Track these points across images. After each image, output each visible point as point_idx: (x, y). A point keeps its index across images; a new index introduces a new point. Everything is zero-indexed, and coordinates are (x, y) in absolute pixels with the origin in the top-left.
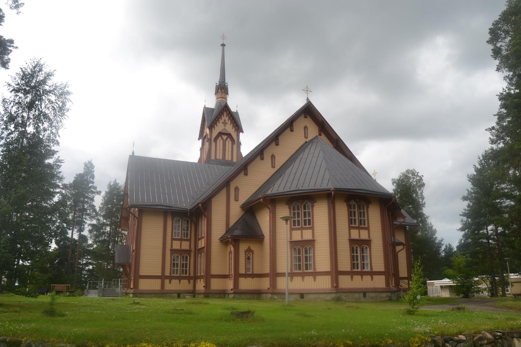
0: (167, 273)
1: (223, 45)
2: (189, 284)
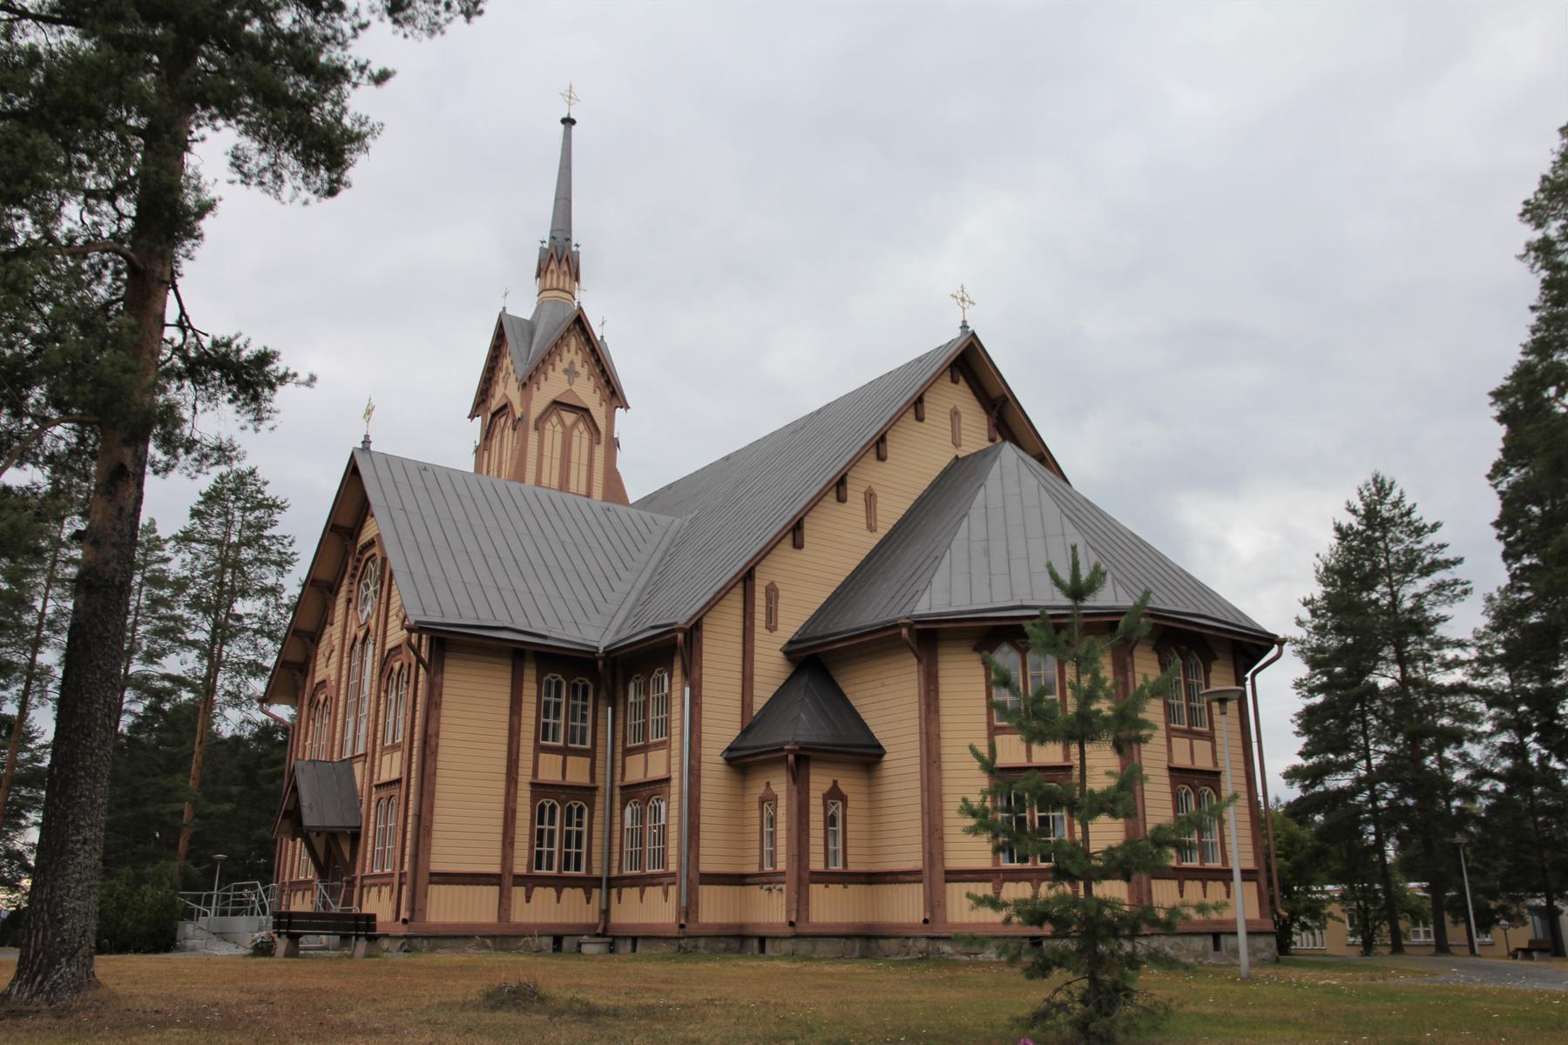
0: (520, 867)
1: (568, 122)
2: (588, 902)
